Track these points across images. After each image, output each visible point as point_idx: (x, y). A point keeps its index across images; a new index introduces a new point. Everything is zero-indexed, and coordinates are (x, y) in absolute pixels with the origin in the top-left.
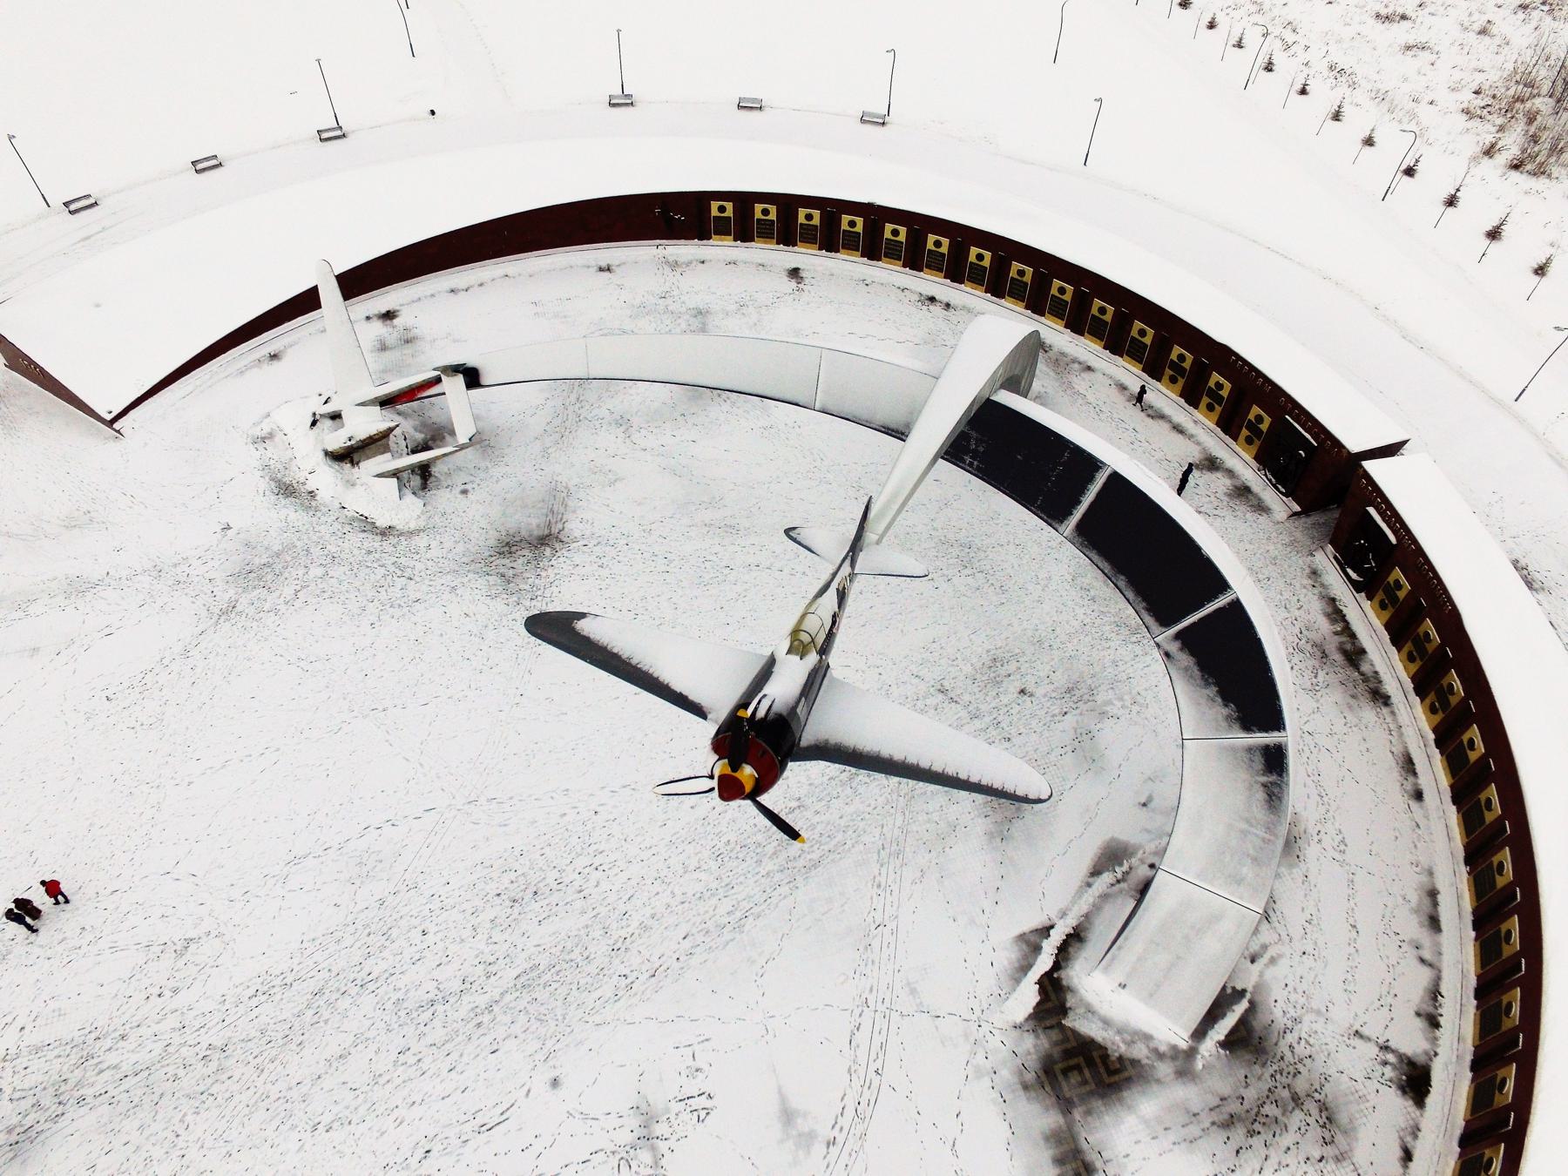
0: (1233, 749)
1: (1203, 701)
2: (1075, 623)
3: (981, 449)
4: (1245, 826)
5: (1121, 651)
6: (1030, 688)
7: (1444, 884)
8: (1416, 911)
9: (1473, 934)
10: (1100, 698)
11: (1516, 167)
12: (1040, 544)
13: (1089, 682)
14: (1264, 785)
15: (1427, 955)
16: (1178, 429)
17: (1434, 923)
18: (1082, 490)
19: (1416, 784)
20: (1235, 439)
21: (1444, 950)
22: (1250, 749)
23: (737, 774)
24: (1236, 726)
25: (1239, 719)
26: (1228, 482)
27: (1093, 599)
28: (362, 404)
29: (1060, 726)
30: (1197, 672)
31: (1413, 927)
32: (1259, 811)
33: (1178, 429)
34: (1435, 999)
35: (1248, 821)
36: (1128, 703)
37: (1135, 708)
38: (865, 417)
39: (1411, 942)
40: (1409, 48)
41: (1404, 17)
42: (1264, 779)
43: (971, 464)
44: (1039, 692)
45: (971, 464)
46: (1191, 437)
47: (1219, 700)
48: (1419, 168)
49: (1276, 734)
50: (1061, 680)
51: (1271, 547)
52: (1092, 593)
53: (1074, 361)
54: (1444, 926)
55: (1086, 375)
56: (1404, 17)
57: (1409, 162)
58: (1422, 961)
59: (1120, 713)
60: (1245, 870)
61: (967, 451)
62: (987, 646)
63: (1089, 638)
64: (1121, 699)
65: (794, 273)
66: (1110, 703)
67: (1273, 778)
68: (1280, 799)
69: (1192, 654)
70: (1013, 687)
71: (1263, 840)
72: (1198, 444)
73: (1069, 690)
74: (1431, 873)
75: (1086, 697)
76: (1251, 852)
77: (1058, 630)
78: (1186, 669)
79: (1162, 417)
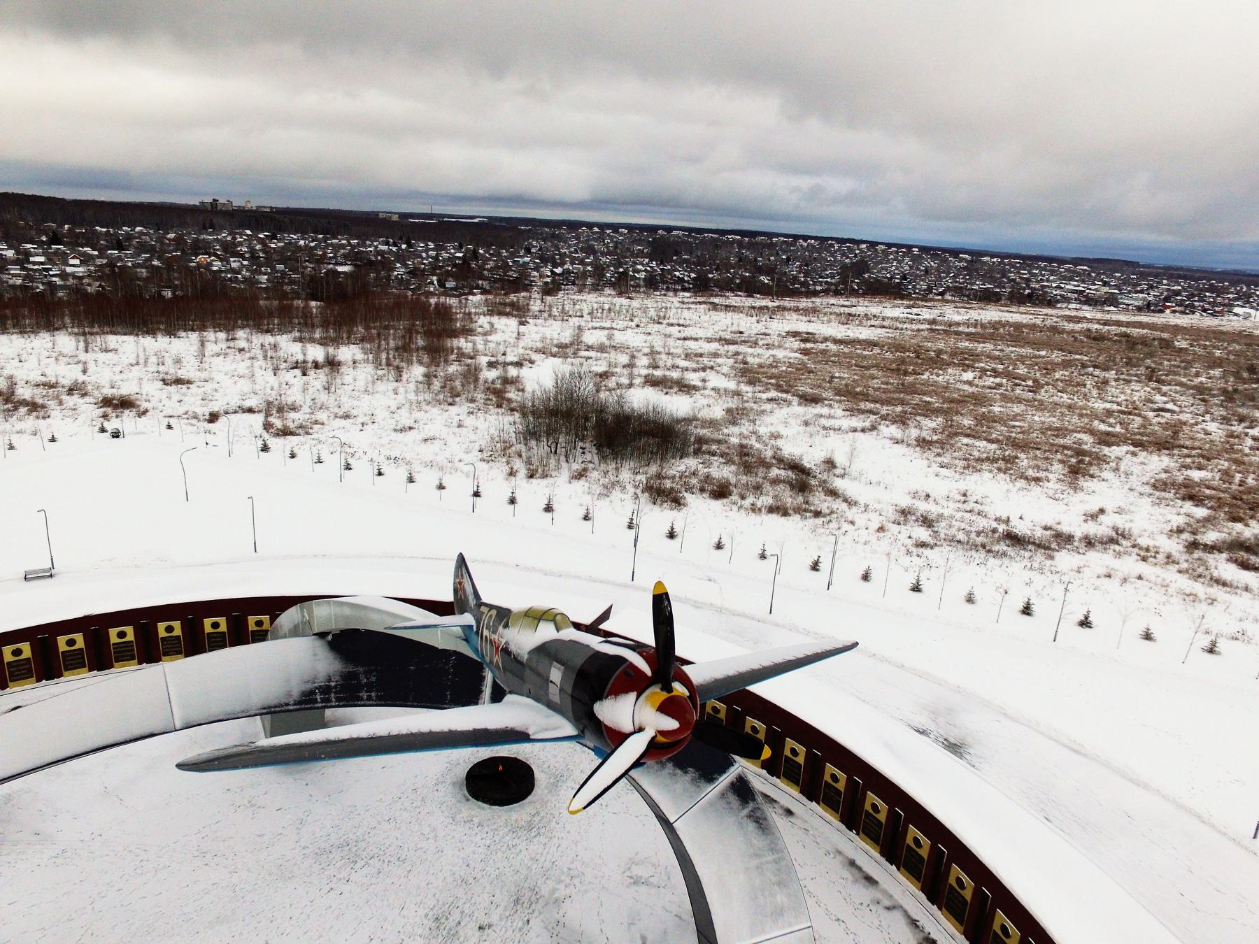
0: (711, 804)
2: (481, 850)
3: (373, 679)
4: (755, 862)
5: (531, 847)
6: (485, 921)
7: (852, 854)
8: (856, 881)
9: (894, 867)
10: (545, 891)
11: (531, 477)
13: (526, 885)
14: (749, 816)
15: (887, 903)
17: (870, 880)
19: (782, 807)
21: (891, 892)
22: (723, 795)
23: (674, 693)
24: (702, 784)
25: (701, 776)
27: (480, 825)
29: (532, 934)
31: (863, 893)
32: (759, 841)
34: (917, 927)
35: (757, 856)
36: (568, 880)
37: (576, 881)
38: (238, 709)
39: (872, 901)
41: (410, 428)
42: (745, 812)
43: (369, 698)
44: (494, 918)
45: (369, 698)
47: (679, 772)
48: (481, 489)
49: (732, 769)
50: (503, 899)
52: (476, 820)
54: (876, 878)
56: (410, 428)
58: (888, 908)
59: (568, 892)
60: (779, 898)
61: (360, 687)
62: (422, 912)
63: (500, 855)
64: (560, 882)
66: (554, 890)
67: (751, 805)
68: (765, 819)
70: (469, 930)
71: (775, 861)
73: (517, 901)
74: (840, 853)
75: (533, 899)
76: (774, 879)
77: (472, 865)
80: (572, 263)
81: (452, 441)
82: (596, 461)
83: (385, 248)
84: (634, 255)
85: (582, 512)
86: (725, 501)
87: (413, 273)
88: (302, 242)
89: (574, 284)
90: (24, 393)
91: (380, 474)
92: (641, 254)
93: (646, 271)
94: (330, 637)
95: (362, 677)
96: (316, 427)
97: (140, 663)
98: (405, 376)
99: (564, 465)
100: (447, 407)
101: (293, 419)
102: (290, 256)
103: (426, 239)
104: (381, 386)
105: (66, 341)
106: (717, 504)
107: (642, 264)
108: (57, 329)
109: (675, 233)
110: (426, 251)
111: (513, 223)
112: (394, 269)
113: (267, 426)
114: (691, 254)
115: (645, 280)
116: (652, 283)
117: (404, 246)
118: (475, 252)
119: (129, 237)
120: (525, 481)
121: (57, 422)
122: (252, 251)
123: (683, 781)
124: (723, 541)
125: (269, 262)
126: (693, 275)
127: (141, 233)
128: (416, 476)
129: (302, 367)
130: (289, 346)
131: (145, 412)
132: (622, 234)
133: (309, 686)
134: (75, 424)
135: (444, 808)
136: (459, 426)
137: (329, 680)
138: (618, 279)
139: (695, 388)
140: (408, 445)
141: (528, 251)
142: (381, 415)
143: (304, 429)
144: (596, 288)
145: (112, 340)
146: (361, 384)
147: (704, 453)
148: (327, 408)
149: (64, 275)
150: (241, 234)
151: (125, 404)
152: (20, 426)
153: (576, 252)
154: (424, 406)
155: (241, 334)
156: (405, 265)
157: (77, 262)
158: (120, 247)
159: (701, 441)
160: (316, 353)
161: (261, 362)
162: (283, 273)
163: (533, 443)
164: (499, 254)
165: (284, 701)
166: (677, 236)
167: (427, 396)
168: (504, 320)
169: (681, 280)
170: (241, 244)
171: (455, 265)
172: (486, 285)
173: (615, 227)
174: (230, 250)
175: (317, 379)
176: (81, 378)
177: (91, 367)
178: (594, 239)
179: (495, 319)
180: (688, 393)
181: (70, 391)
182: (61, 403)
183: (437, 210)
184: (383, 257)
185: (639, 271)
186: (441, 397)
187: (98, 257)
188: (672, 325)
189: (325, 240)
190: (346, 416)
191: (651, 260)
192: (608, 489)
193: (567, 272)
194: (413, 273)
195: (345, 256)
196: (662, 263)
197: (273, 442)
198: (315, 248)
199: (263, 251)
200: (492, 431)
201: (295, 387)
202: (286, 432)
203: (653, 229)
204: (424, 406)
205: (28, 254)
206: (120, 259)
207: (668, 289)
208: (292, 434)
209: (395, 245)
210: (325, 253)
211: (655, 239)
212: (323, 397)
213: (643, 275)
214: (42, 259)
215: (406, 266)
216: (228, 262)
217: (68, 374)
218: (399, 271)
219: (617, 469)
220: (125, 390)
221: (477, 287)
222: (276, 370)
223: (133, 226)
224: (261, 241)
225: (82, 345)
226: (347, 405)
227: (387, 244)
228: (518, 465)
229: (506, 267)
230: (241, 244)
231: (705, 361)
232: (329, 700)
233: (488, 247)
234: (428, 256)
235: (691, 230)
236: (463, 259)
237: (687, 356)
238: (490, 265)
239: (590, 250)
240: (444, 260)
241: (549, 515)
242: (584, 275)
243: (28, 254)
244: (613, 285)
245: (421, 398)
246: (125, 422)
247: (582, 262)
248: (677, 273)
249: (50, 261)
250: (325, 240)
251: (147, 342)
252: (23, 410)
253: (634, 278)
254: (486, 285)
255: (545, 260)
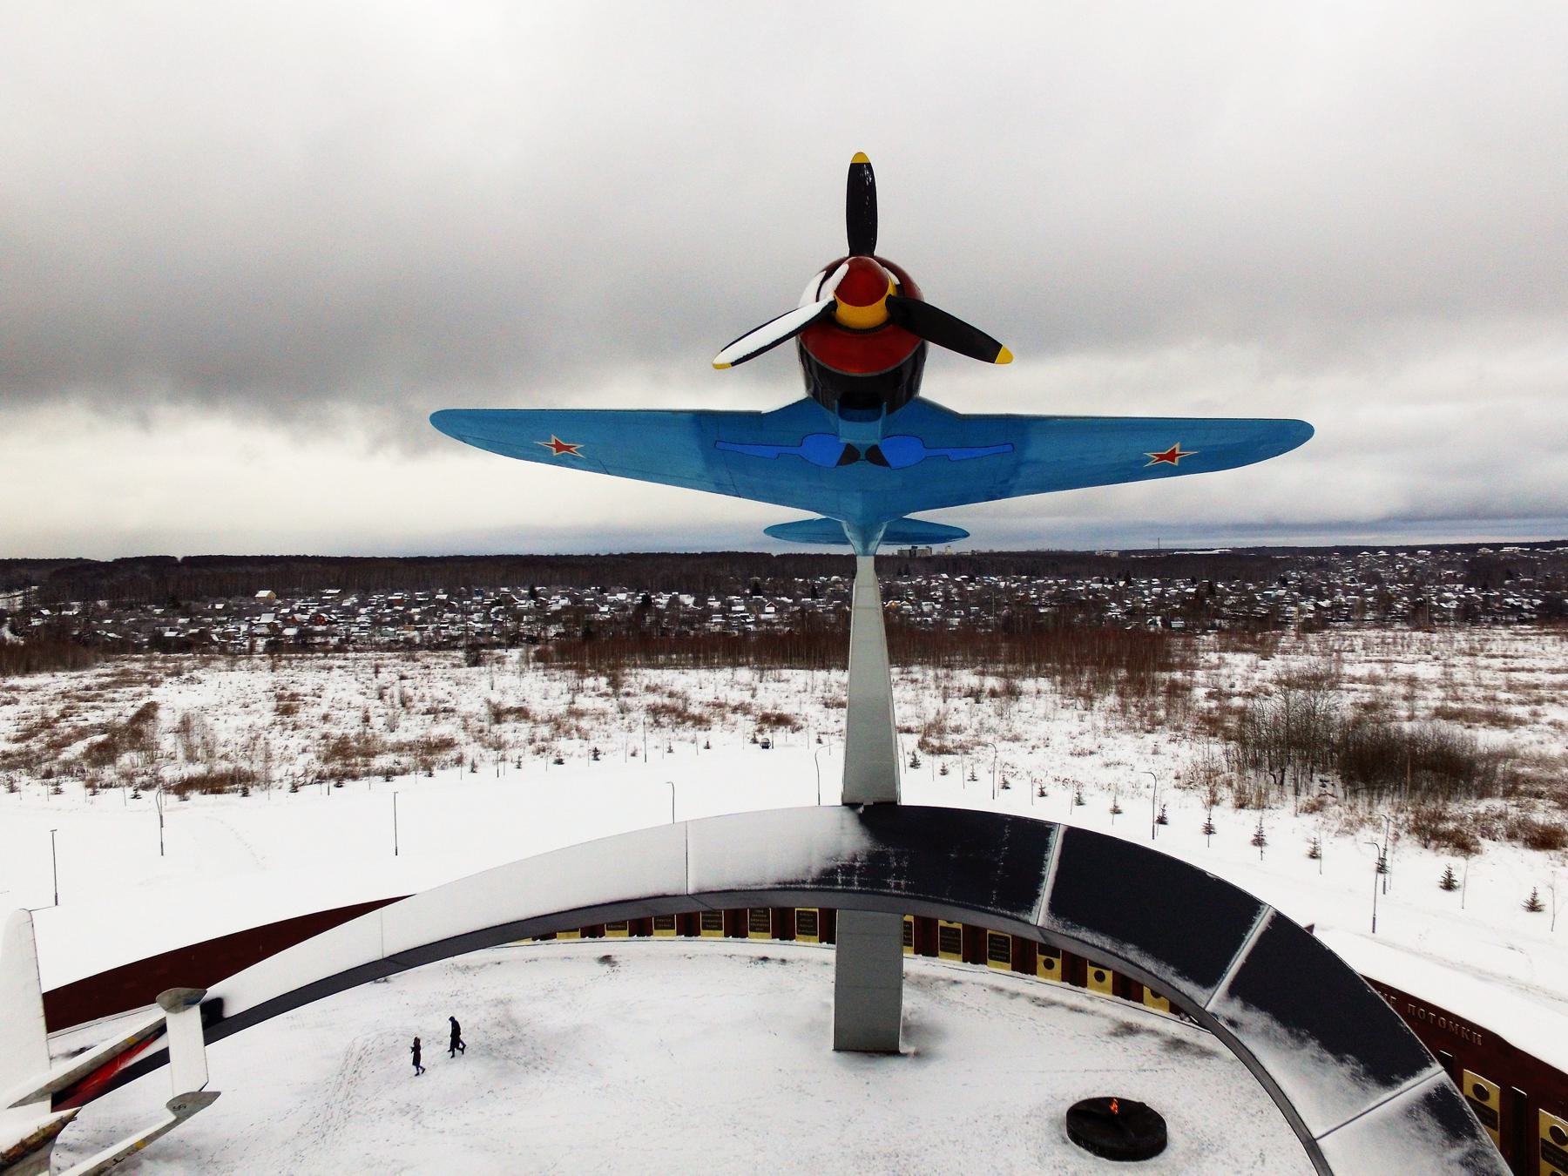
0: (1388, 1122)
1: (1310, 1068)
3: (905, 864)
11: (1242, 806)
12: (980, 1135)
14: (1464, 1163)
16: (1074, 1009)
18: (1040, 863)
20: (1140, 1000)
22: (1409, 1113)
24: (1372, 1086)
26: (1156, 1040)
28: (23, 1102)
30: (1281, 1032)
33: (1074, 1009)
40: (1107, 765)
42: (1456, 1153)
46: (1093, 1013)
47: (1329, 1056)
48: (1168, 815)
51: (1243, 1084)
53: (937, 979)
55: (954, 988)
56: (1091, 753)
57: (1158, 813)
65: (606, 959)
69: (1262, 1007)
72: (1104, 1016)
78: (1265, 1032)
79: (1053, 1004)
80: (1345, 595)
81: (1142, 766)
82: (1341, 794)
83: (1096, 586)
84: (1439, 581)
85: (1308, 847)
86: (1552, 853)
87: (1131, 613)
88: (1002, 584)
89: (1347, 619)
90: (695, 710)
91: (1043, 794)
92: (1453, 579)
93: (1458, 599)
94: (861, 810)
95: (892, 859)
96: (978, 748)
97: (726, 935)
98: (1097, 705)
99: (1291, 797)
100: (1142, 734)
101: (950, 740)
102: (987, 600)
103: (1150, 576)
104: (1066, 714)
105: (744, 674)
106: (1540, 857)
107: (1453, 591)
108: (741, 665)
109: (1506, 549)
110: (1150, 589)
111: (1263, 554)
112: (1109, 609)
113: (922, 745)
114: (1534, 574)
115: (1455, 611)
116: (1468, 615)
117: (1122, 583)
118: (1212, 591)
119: (824, 586)
120: (1231, 811)
121: (717, 733)
122: (947, 594)
123: (1337, 1074)
124: (1541, 899)
125: (964, 604)
126: (1538, 602)
127: (837, 582)
128: (1085, 798)
129: (976, 695)
130: (966, 678)
131: (799, 729)
132: (1421, 557)
133: (832, 864)
134: (730, 739)
135: (1030, 1144)
136: (1155, 753)
137: (855, 859)
138: (1415, 612)
139: (1519, 722)
140: (1085, 770)
141: (1284, 582)
142: (1059, 739)
143: (964, 749)
144: (1380, 624)
145: (786, 673)
146: (1040, 711)
147: (1522, 794)
148: (995, 731)
149: (758, 622)
150: (937, 579)
151: (782, 721)
152: (686, 735)
153: (1353, 581)
154: (1114, 733)
155: (915, 669)
156: (1121, 604)
157: (772, 609)
158: (814, 595)
159: (1515, 779)
160: (992, 682)
161: (933, 691)
162: (977, 614)
163: (1251, 773)
164: (1244, 587)
165: (801, 877)
166: (1512, 554)
167: (1121, 723)
168: (1239, 656)
169: (1516, 610)
170: (936, 589)
171: (1184, 602)
172: (1225, 624)
173: (1412, 550)
174: (923, 593)
175: (988, 706)
176: (748, 699)
177: (760, 693)
178: (1380, 566)
179: (1229, 656)
180: (1505, 727)
181: (735, 710)
182: (724, 719)
183: (1167, 544)
184: (1095, 596)
185: (1447, 600)
186: (1138, 725)
187: (793, 605)
188: (1494, 657)
189: (1029, 581)
190: (1016, 739)
191: (1468, 586)
192: (1350, 828)
193: (1337, 607)
194: (1131, 613)
195: (1050, 597)
196: (1485, 588)
197: (923, 757)
198: (1017, 589)
199: (959, 595)
200: (1199, 759)
201: (961, 712)
202: (942, 751)
203: (1474, 548)
204: (1114, 733)
205: (731, 604)
206: (813, 606)
207: (1495, 622)
208: (949, 752)
209: (1111, 582)
210: (1028, 594)
211: (1473, 560)
212: (994, 722)
213: (1454, 605)
214: (742, 608)
215: (1123, 605)
216: (920, 606)
217: (735, 697)
218: (1115, 611)
219: (1370, 804)
220: (786, 710)
221: (1213, 627)
222: (945, 698)
223: (829, 575)
224: (958, 585)
225: (757, 677)
226: (1018, 727)
227: (1102, 582)
228: (1226, 794)
229: (1252, 602)
230: (936, 589)
231: (1543, 693)
232: (850, 883)
233: (1228, 579)
234: (1151, 594)
235: (1533, 546)
236: (1196, 594)
237: (1511, 688)
238: (1232, 599)
239: (1373, 578)
240: (1171, 597)
241: (1258, 849)
242: (1363, 608)
243: (731, 604)
244: (1405, 619)
245: (1111, 725)
246: (780, 736)
247: (1359, 592)
248: (1510, 600)
249: (749, 609)
250: (1029, 581)
251: (821, 675)
252: (689, 723)
253: (1439, 609)
254: (1225, 624)
255: (1305, 591)
